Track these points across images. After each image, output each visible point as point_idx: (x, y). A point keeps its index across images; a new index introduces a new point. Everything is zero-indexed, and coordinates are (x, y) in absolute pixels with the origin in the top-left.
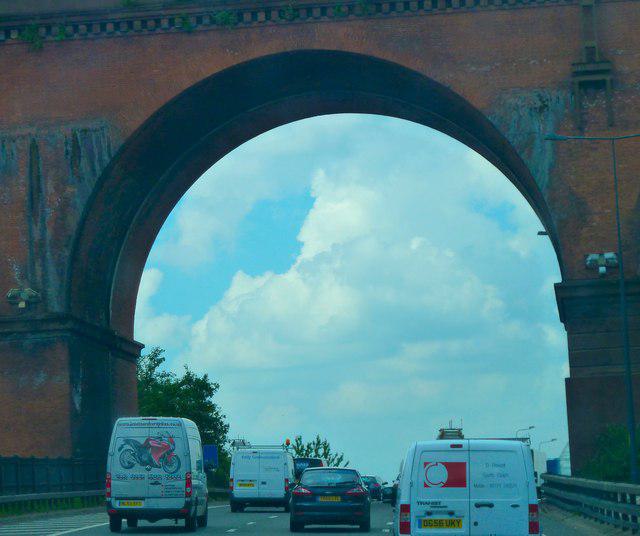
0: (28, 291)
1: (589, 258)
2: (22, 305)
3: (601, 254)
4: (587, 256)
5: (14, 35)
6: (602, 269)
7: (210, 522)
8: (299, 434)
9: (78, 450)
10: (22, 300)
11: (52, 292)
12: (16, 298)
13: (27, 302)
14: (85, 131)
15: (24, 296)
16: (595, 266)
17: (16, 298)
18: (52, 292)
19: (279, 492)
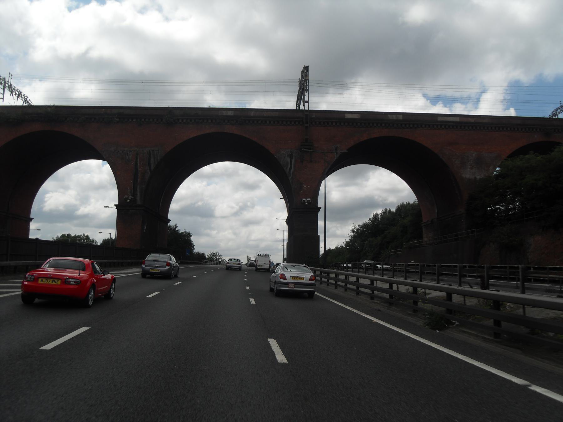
0: (131, 197)
1: (303, 200)
2: (128, 201)
3: (306, 199)
4: (302, 199)
5: (134, 120)
6: (306, 203)
7: (179, 276)
8: (41, 229)
9: (359, 231)
10: (128, 199)
11: (138, 197)
12: (127, 199)
13: (130, 200)
14: (153, 151)
15: (130, 198)
16: (304, 202)
17: (127, 199)
18: (138, 197)
19: (3, 90)
